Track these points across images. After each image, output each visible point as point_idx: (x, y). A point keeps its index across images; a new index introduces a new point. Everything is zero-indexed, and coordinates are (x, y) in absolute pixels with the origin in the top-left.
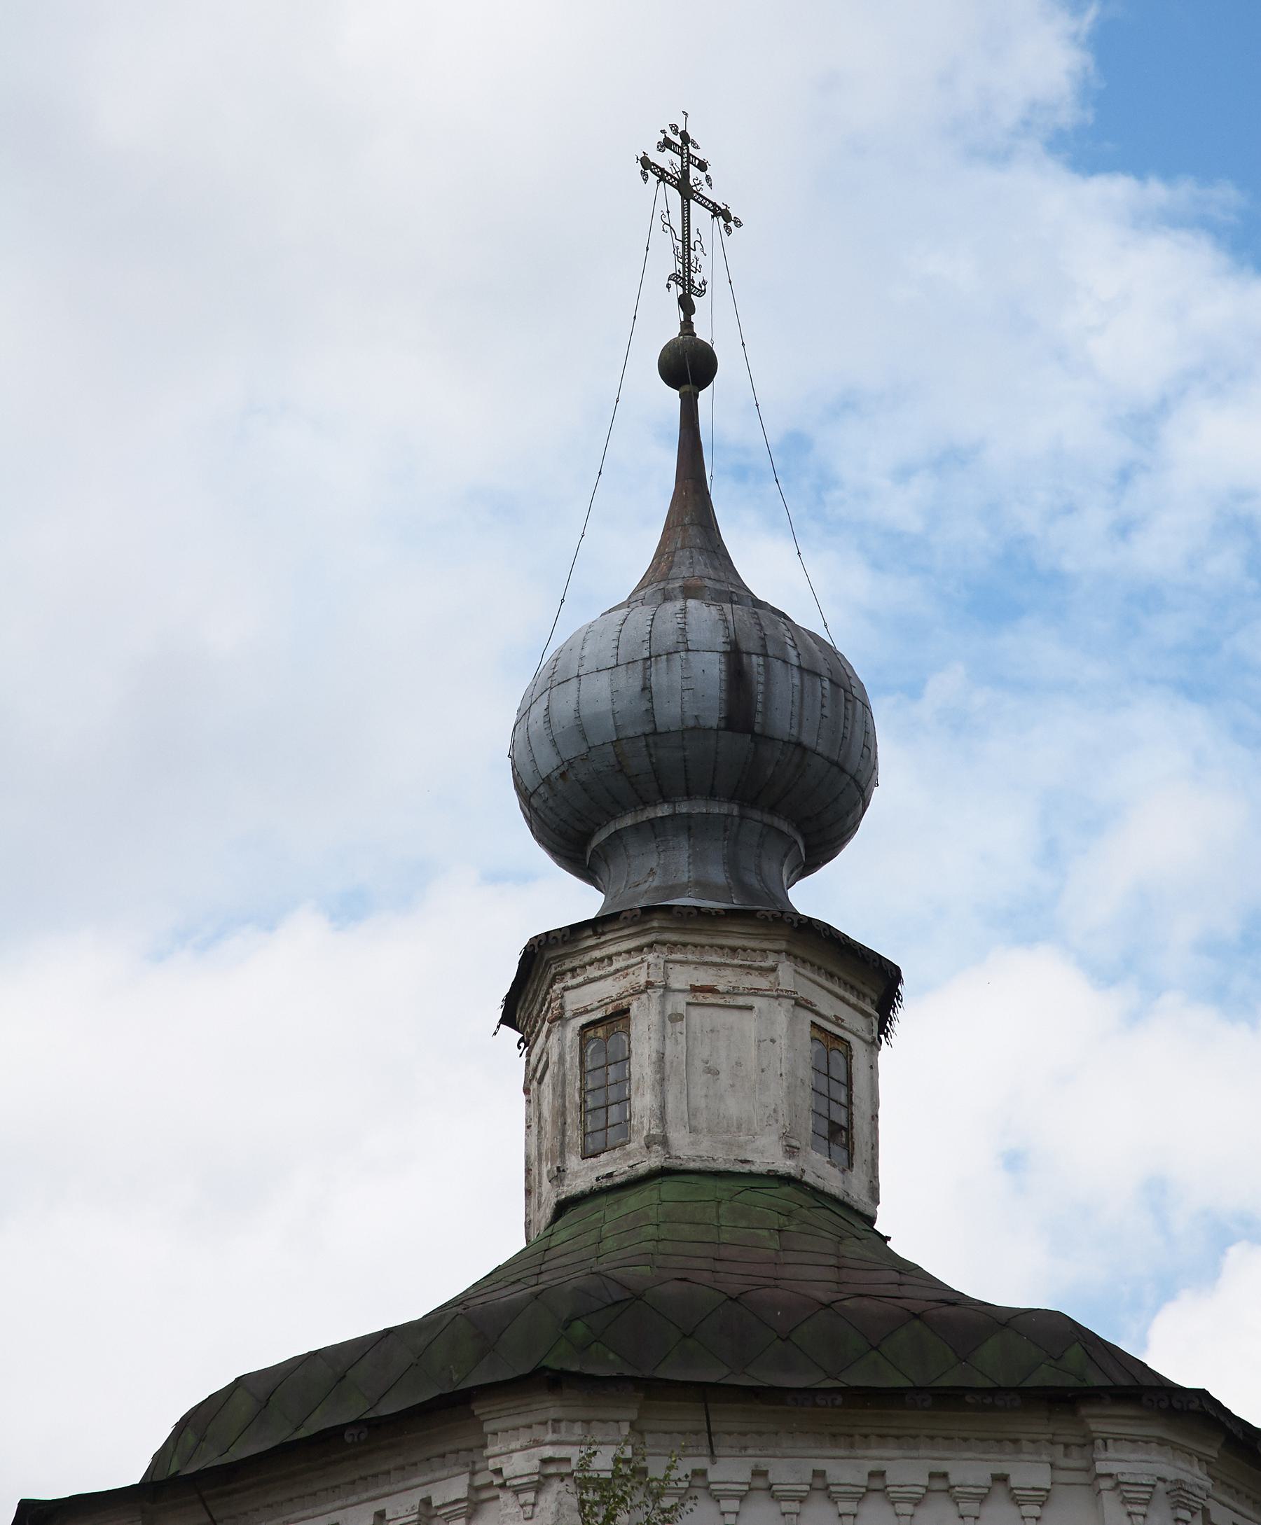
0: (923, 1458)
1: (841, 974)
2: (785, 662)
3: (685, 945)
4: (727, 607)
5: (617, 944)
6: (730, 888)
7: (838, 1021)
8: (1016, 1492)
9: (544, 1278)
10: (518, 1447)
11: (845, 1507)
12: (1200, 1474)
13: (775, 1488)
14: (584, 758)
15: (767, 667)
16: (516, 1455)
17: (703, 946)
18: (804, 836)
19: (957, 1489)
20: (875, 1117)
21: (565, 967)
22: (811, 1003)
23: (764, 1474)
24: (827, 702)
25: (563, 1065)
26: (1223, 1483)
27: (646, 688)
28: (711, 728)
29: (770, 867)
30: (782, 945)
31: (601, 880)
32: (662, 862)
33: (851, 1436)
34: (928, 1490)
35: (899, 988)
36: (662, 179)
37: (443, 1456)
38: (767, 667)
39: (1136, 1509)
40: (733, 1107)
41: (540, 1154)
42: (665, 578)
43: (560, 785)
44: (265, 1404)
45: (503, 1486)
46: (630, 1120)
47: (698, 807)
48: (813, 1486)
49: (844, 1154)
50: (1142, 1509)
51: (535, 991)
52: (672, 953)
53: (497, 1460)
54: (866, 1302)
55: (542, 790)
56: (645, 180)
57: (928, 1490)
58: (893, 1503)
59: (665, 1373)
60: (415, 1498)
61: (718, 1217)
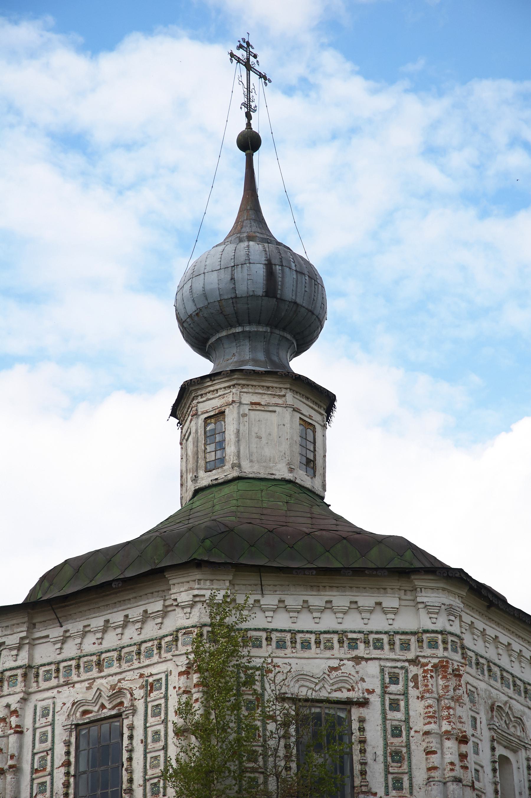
0: (347, 596)
1: (311, 398)
2: (290, 268)
3: (248, 385)
4: (266, 245)
5: (220, 384)
6: (266, 362)
7: (310, 417)
8: (385, 609)
9: (190, 521)
10: (184, 590)
11: (315, 615)
12: (459, 602)
13: (287, 607)
14: (206, 307)
15: (282, 270)
16: (182, 593)
17: (255, 386)
18: (297, 341)
19: (361, 608)
20: (325, 456)
21: (198, 394)
22: (299, 410)
23: (283, 601)
24: (307, 285)
25: (197, 434)
26: (467, 605)
27: (232, 279)
28: (259, 296)
29: (282, 354)
30: (288, 386)
31: (212, 357)
32: (238, 351)
33: (319, 586)
34: (349, 608)
35: (335, 403)
36: (239, 62)
37: (152, 593)
38: (282, 270)
39: (433, 616)
40: (268, 452)
41: (187, 470)
42: (240, 232)
43: (196, 318)
44: (77, 571)
45: (177, 606)
46: (225, 457)
47: (253, 328)
48: (303, 606)
49: (312, 471)
50: (435, 616)
51: (185, 404)
52: (243, 388)
53: (175, 595)
54: (324, 533)
55: (188, 320)
56: (232, 62)
57: (349, 608)
58: (335, 613)
59: (243, 561)
60: (141, 610)
61: (262, 497)
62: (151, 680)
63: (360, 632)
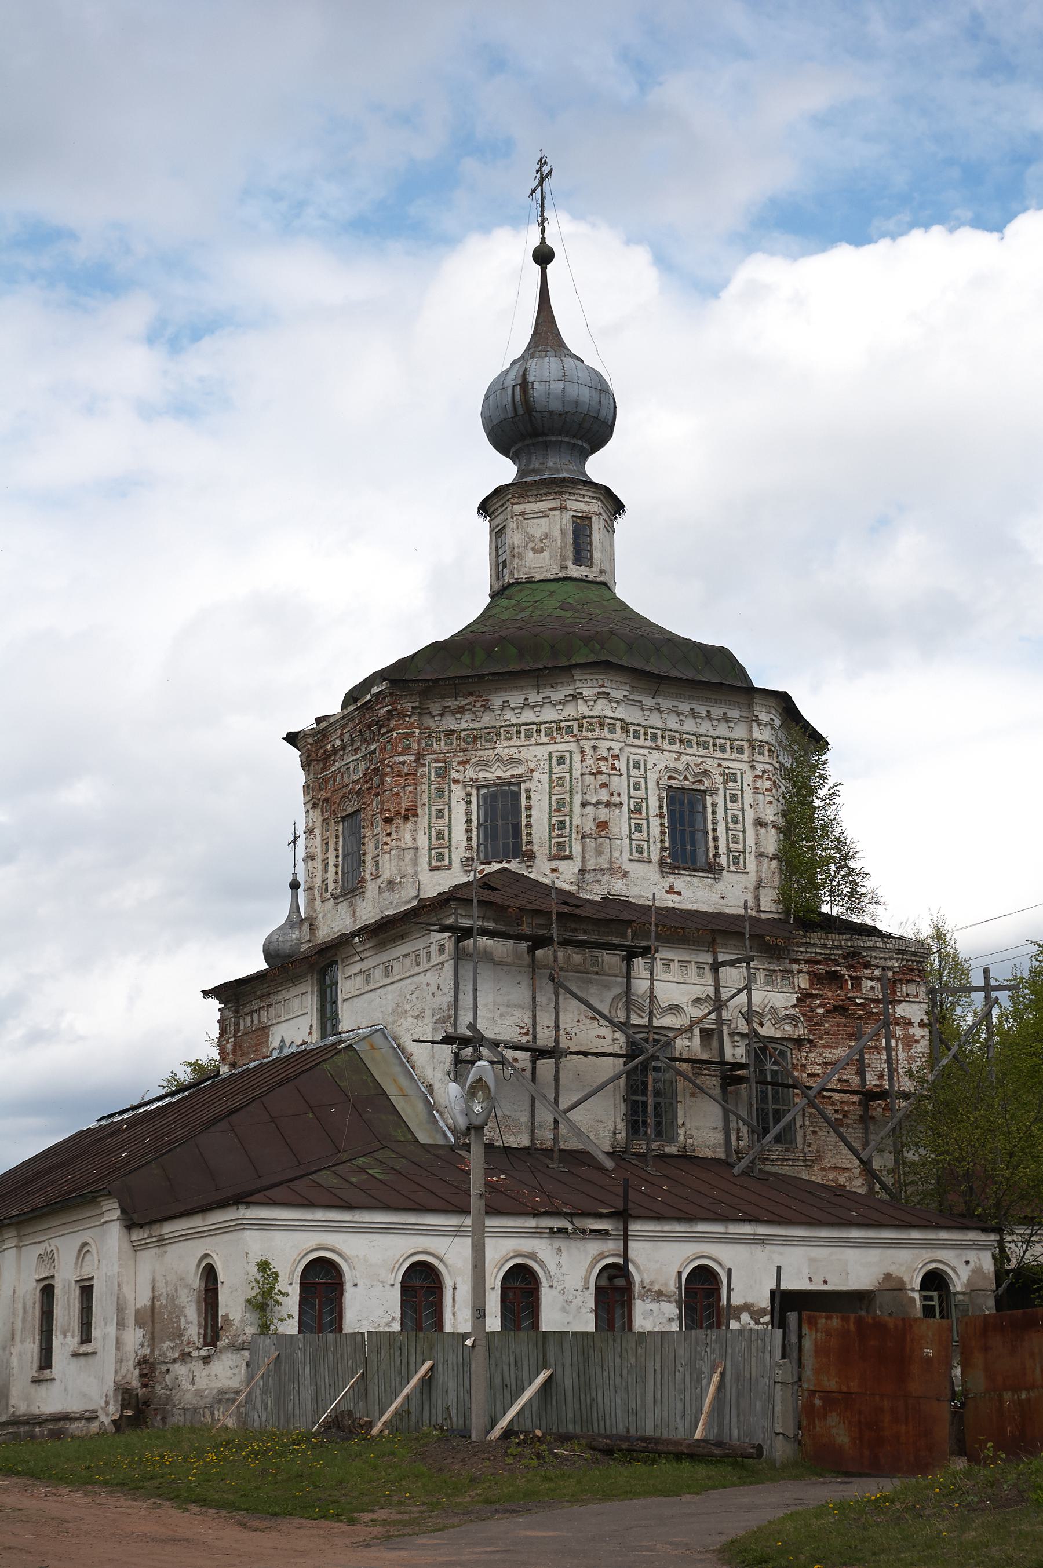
14: (573, 414)
60: (722, 711)
62: (727, 771)
63: (492, 727)
